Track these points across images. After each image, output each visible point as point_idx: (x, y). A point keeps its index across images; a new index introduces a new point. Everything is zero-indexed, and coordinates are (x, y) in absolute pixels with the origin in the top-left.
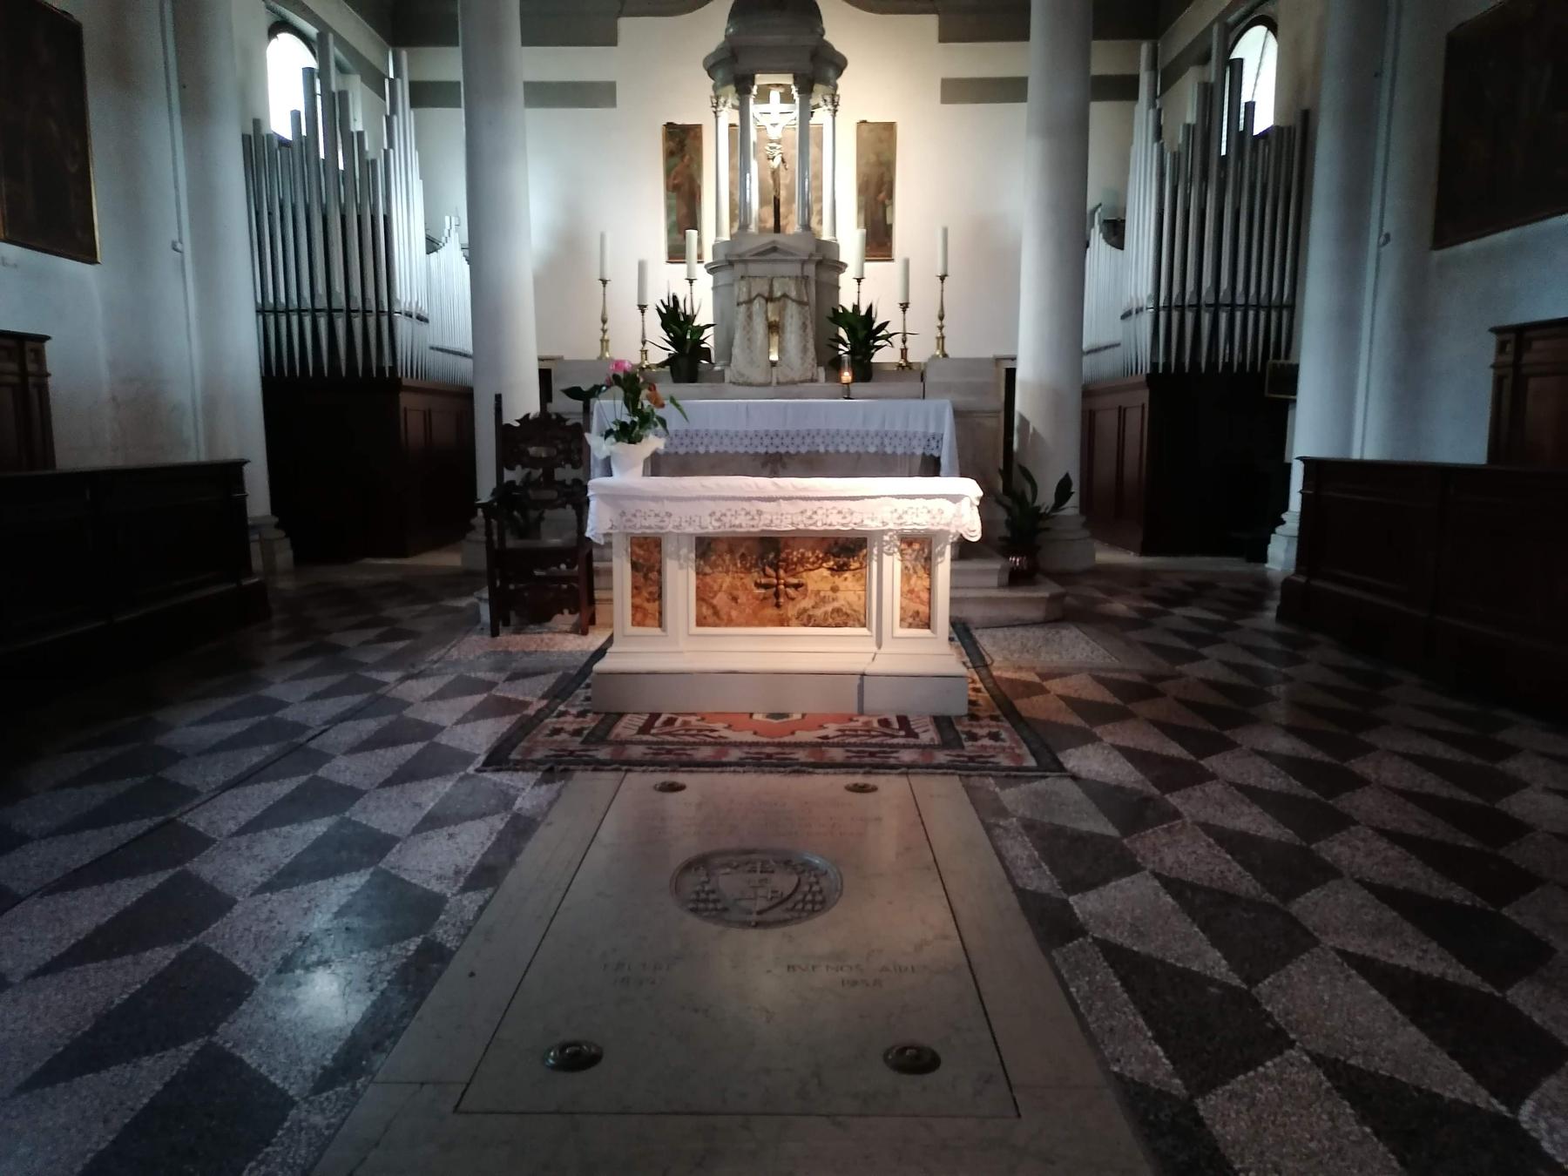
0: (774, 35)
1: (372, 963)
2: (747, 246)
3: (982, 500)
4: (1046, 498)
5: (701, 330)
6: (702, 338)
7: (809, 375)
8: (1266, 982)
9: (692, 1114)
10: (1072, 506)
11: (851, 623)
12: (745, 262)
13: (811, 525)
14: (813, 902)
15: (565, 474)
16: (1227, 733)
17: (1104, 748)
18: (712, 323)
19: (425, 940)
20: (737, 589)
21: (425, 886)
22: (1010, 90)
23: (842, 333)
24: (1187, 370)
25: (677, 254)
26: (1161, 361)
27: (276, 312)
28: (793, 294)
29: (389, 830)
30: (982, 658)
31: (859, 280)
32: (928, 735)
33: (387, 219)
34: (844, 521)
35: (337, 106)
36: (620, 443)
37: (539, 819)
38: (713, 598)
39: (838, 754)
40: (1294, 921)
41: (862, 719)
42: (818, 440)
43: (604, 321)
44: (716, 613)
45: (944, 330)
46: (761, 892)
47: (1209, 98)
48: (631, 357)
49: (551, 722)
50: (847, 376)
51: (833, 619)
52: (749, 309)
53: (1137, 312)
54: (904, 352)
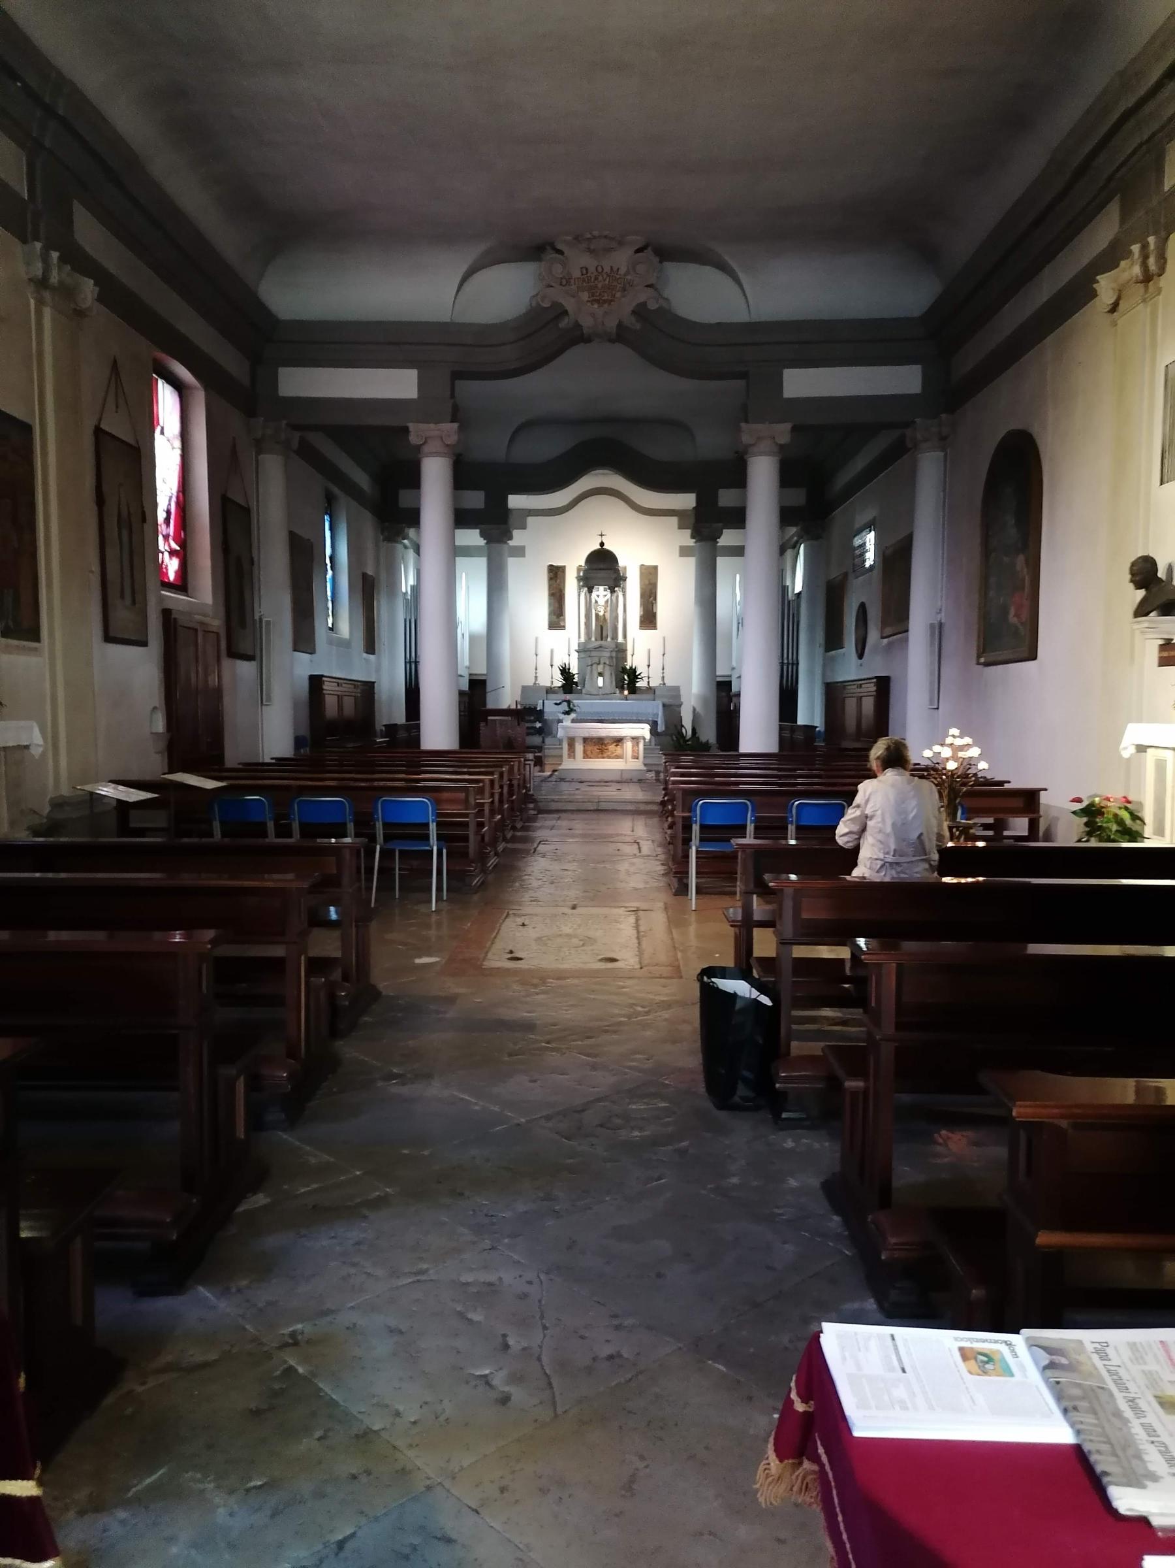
7: (613, 692)
23: (626, 677)
28: (608, 663)
43: (536, 669)
44: (587, 755)
50: (626, 692)
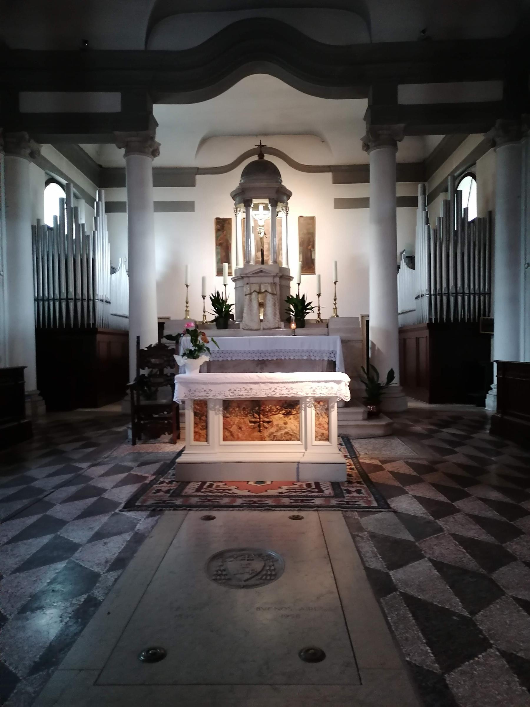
0: (261, 182)
1: (63, 608)
2: (250, 270)
3: (350, 383)
4: (383, 379)
5: (229, 306)
6: (230, 310)
7: (277, 325)
8: (479, 614)
9: (207, 684)
10: (396, 382)
11: (293, 439)
12: (248, 277)
13: (274, 394)
14: (271, 575)
15: (168, 371)
16: (466, 489)
17: (409, 497)
18: (234, 303)
19: (89, 596)
20: (241, 424)
21: (91, 568)
22: (363, 203)
23: (292, 307)
24: (445, 322)
25: (220, 272)
26: (433, 318)
27: (43, 300)
28: (270, 290)
29: (76, 541)
30: (355, 453)
31: (299, 284)
32: (328, 491)
33: (94, 260)
34: (289, 393)
35: (73, 213)
36: (189, 359)
37: (146, 535)
38: (230, 428)
39: (286, 501)
40: (493, 582)
41: (299, 484)
42: (281, 354)
43: (187, 303)
44: (232, 435)
45: (336, 305)
46: (247, 570)
47: (448, 206)
48: (199, 318)
49: (156, 486)
50: (293, 326)
51: (285, 437)
52: (250, 297)
53: (422, 297)
54: (319, 315)
